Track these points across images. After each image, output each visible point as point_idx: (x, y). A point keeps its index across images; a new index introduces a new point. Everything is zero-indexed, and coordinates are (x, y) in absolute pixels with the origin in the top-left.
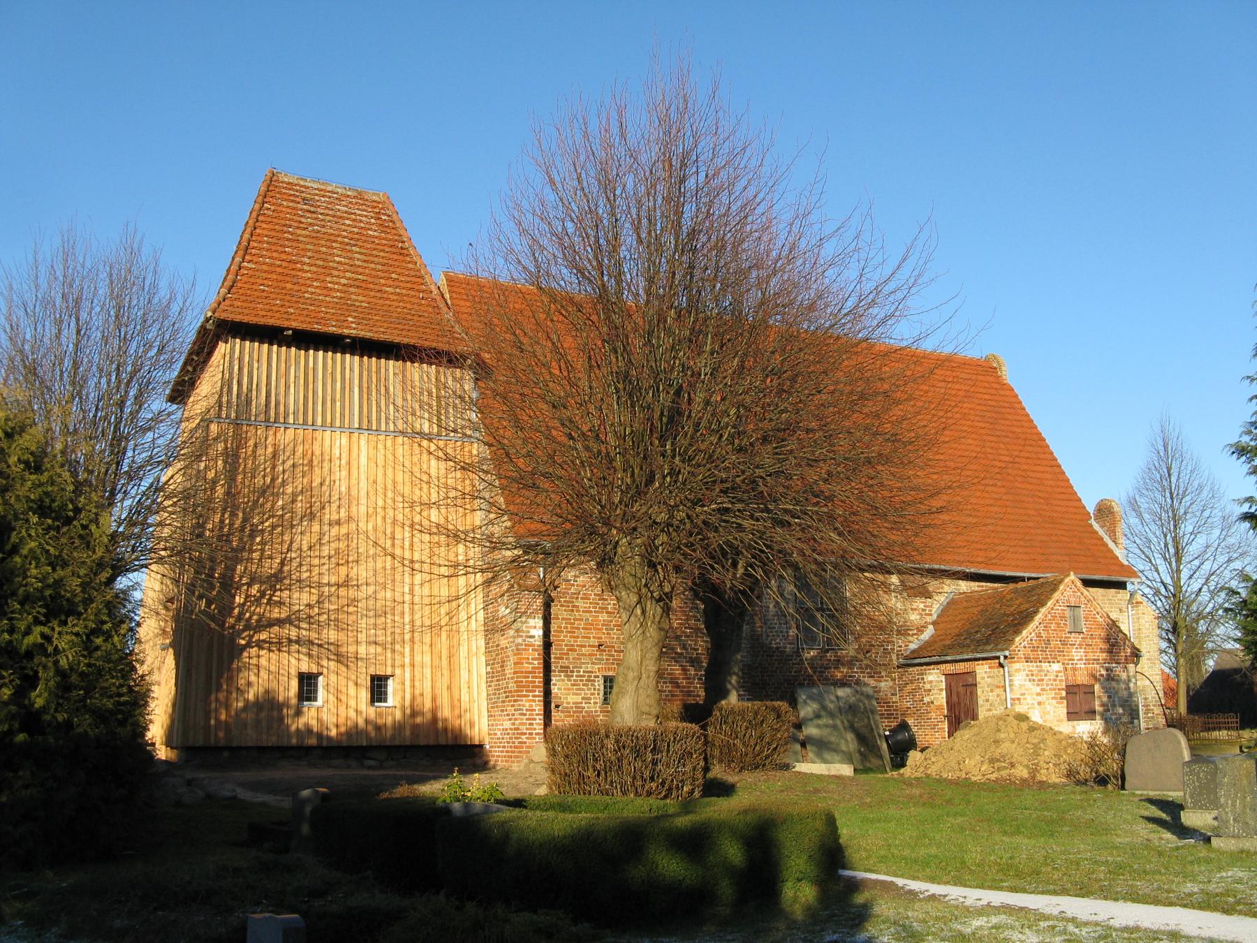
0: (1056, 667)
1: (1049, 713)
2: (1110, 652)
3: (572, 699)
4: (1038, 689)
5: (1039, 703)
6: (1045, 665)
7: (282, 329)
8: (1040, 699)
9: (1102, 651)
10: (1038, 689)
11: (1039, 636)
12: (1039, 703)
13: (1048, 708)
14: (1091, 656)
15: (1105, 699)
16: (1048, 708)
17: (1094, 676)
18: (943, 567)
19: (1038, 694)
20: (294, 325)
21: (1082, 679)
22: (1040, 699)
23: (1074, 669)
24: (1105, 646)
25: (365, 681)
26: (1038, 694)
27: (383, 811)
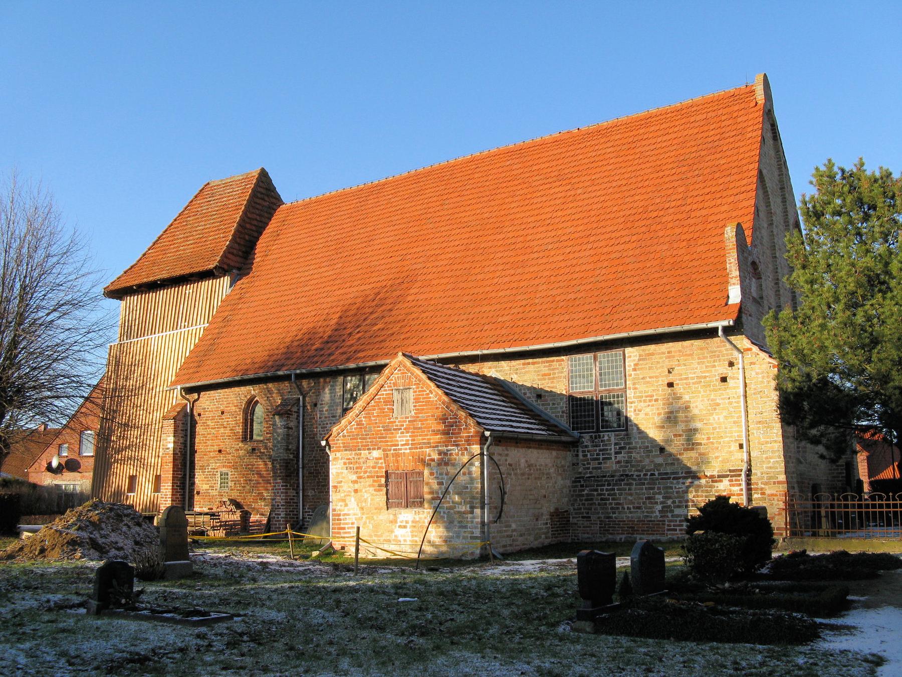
0: (376, 454)
1: (366, 500)
2: (446, 433)
3: (205, 487)
4: (354, 477)
5: (356, 491)
6: (364, 453)
7: (131, 287)
8: (356, 486)
9: (435, 433)
10: (354, 477)
11: (359, 424)
12: (356, 491)
13: (366, 495)
14: (419, 439)
15: (435, 486)
16: (366, 495)
17: (423, 461)
18: (485, 352)
19: (355, 482)
20: (136, 282)
21: (407, 465)
22: (356, 486)
23: (397, 455)
24: (442, 427)
25: (152, 478)
26: (355, 482)
27: (770, 553)
